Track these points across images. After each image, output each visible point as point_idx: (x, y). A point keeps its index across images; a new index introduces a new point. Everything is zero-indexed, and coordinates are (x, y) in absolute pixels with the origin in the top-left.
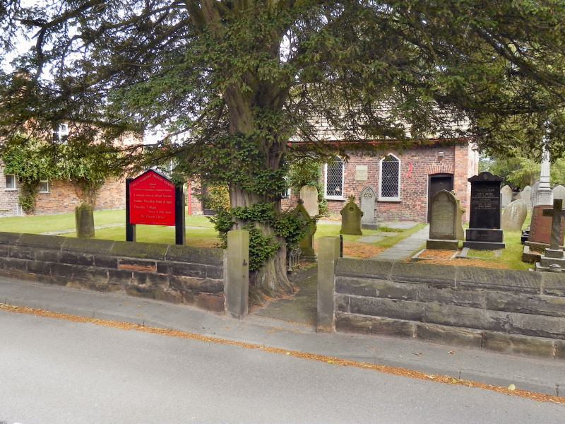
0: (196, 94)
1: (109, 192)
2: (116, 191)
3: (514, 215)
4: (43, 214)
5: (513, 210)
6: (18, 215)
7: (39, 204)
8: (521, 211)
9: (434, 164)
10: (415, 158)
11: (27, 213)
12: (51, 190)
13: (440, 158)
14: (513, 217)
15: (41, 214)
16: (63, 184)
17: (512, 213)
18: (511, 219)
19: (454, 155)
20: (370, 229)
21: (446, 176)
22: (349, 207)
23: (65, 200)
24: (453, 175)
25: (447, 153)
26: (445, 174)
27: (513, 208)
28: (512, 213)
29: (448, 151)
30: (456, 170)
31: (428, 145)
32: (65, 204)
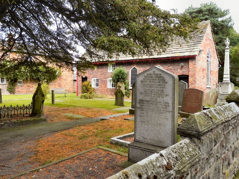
0: (9, 12)
1: (54, 86)
2: (58, 85)
3: (212, 98)
4: (19, 94)
5: (211, 95)
6: (6, 94)
7: (16, 90)
8: (215, 95)
9: (179, 70)
10: (170, 67)
11: (11, 94)
12: (24, 84)
13: (182, 67)
14: (211, 99)
15: (18, 94)
16: (30, 82)
17: (210, 96)
18: (210, 99)
19: (189, 65)
20: (219, 75)
21: (185, 76)
22: (118, 91)
23: (31, 89)
24: (188, 76)
25: (186, 64)
26: (185, 75)
27: (211, 93)
28: (210, 96)
29: (186, 63)
30: (190, 73)
31: (176, 60)
32: (31, 90)
